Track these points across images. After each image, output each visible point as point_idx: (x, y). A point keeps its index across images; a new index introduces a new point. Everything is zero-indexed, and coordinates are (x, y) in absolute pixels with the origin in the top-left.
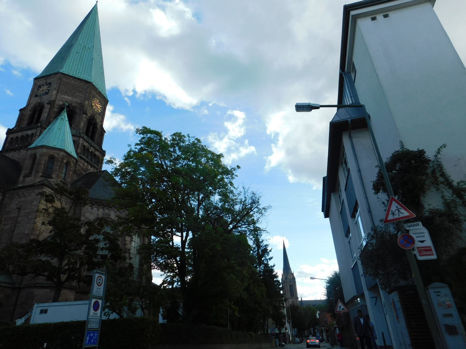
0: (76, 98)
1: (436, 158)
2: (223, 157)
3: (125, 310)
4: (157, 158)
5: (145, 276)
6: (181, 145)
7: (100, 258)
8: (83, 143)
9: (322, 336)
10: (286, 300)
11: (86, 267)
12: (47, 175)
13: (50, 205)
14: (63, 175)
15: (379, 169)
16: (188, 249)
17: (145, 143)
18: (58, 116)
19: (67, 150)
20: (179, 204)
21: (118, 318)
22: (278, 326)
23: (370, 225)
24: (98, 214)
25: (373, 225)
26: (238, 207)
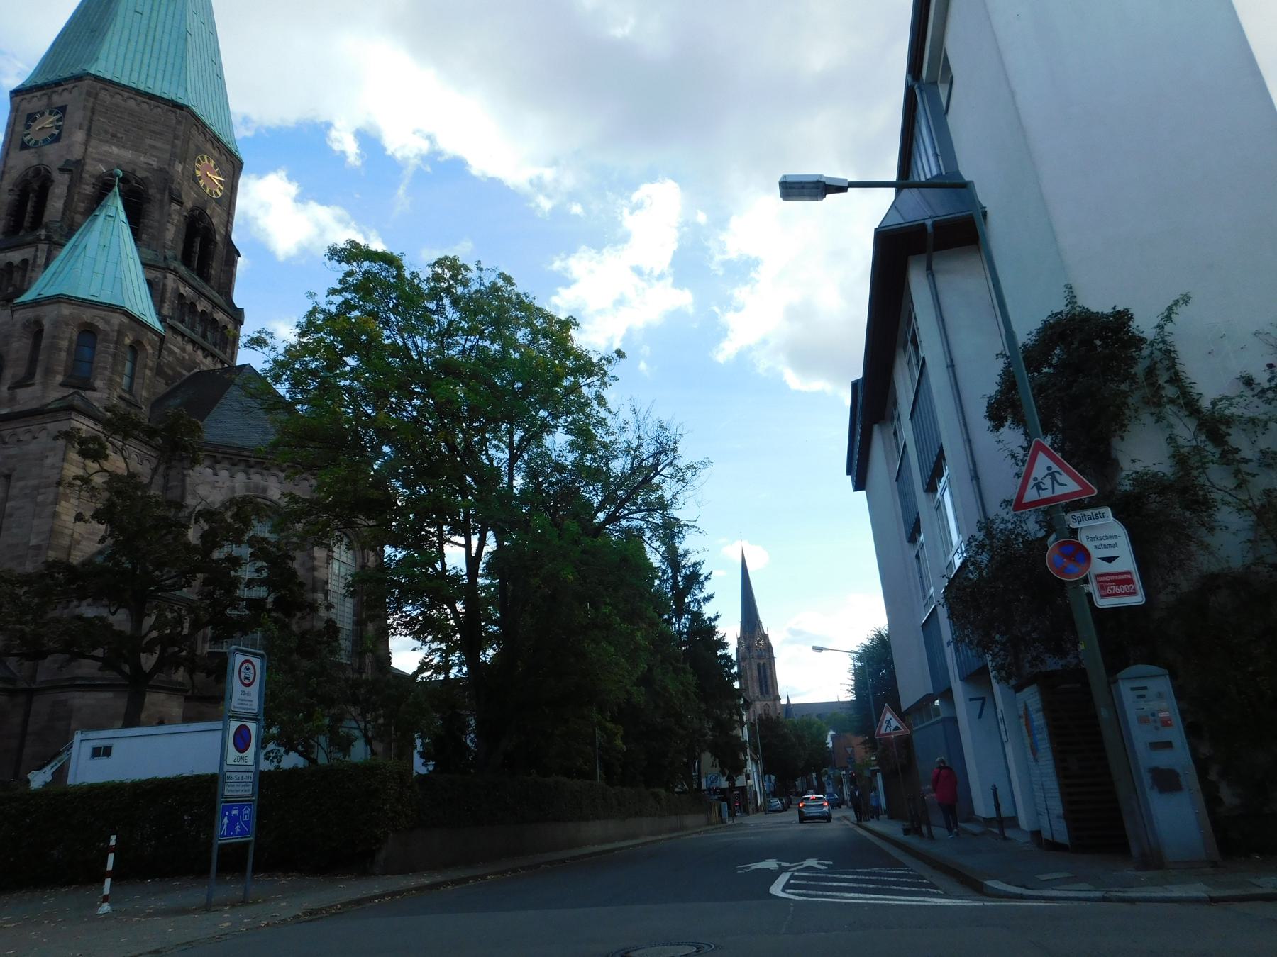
0: (146, 154)
1: (1160, 332)
2: (576, 327)
3: (320, 745)
4: (390, 330)
5: (370, 654)
6: (459, 293)
7: (245, 608)
8: (178, 289)
9: (840, 793)
10: (747, 705)
11: (209, 631)
12: (79, 380)
13: (96, 466)
14: (125, 381)
15: (1006, 361)
16: (486, 579)
17: (356, 288)
18: (96, 208)
19: (131, 309)
20: (458, 459)
21: (302, 767)
22: (727, 772)
23: (975, 516)
24: (233, 489)
25: (982, 516)
26: (618, 466)
